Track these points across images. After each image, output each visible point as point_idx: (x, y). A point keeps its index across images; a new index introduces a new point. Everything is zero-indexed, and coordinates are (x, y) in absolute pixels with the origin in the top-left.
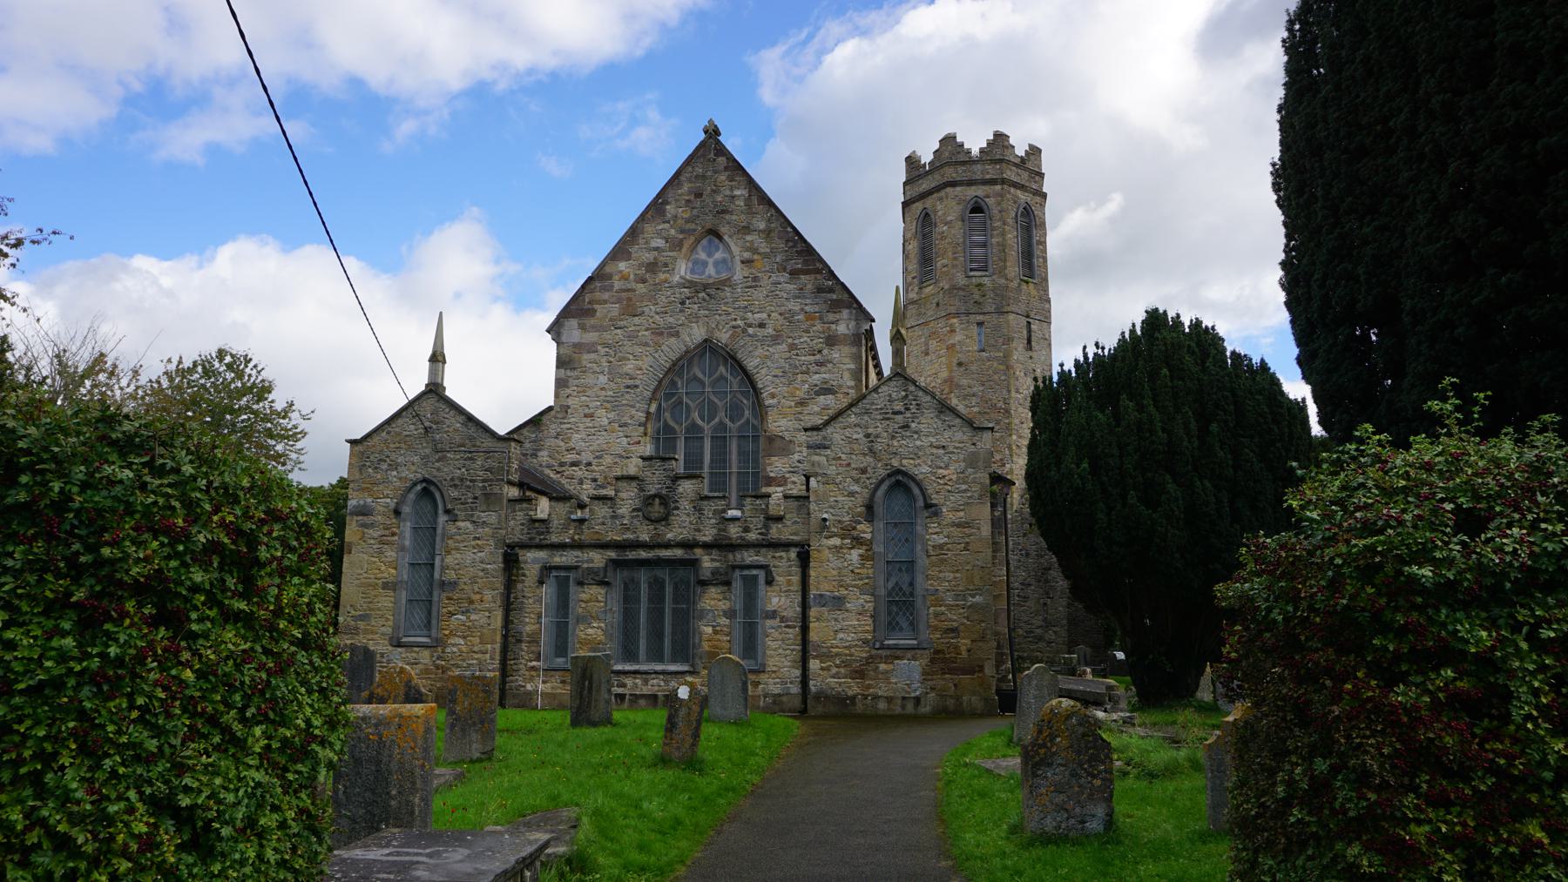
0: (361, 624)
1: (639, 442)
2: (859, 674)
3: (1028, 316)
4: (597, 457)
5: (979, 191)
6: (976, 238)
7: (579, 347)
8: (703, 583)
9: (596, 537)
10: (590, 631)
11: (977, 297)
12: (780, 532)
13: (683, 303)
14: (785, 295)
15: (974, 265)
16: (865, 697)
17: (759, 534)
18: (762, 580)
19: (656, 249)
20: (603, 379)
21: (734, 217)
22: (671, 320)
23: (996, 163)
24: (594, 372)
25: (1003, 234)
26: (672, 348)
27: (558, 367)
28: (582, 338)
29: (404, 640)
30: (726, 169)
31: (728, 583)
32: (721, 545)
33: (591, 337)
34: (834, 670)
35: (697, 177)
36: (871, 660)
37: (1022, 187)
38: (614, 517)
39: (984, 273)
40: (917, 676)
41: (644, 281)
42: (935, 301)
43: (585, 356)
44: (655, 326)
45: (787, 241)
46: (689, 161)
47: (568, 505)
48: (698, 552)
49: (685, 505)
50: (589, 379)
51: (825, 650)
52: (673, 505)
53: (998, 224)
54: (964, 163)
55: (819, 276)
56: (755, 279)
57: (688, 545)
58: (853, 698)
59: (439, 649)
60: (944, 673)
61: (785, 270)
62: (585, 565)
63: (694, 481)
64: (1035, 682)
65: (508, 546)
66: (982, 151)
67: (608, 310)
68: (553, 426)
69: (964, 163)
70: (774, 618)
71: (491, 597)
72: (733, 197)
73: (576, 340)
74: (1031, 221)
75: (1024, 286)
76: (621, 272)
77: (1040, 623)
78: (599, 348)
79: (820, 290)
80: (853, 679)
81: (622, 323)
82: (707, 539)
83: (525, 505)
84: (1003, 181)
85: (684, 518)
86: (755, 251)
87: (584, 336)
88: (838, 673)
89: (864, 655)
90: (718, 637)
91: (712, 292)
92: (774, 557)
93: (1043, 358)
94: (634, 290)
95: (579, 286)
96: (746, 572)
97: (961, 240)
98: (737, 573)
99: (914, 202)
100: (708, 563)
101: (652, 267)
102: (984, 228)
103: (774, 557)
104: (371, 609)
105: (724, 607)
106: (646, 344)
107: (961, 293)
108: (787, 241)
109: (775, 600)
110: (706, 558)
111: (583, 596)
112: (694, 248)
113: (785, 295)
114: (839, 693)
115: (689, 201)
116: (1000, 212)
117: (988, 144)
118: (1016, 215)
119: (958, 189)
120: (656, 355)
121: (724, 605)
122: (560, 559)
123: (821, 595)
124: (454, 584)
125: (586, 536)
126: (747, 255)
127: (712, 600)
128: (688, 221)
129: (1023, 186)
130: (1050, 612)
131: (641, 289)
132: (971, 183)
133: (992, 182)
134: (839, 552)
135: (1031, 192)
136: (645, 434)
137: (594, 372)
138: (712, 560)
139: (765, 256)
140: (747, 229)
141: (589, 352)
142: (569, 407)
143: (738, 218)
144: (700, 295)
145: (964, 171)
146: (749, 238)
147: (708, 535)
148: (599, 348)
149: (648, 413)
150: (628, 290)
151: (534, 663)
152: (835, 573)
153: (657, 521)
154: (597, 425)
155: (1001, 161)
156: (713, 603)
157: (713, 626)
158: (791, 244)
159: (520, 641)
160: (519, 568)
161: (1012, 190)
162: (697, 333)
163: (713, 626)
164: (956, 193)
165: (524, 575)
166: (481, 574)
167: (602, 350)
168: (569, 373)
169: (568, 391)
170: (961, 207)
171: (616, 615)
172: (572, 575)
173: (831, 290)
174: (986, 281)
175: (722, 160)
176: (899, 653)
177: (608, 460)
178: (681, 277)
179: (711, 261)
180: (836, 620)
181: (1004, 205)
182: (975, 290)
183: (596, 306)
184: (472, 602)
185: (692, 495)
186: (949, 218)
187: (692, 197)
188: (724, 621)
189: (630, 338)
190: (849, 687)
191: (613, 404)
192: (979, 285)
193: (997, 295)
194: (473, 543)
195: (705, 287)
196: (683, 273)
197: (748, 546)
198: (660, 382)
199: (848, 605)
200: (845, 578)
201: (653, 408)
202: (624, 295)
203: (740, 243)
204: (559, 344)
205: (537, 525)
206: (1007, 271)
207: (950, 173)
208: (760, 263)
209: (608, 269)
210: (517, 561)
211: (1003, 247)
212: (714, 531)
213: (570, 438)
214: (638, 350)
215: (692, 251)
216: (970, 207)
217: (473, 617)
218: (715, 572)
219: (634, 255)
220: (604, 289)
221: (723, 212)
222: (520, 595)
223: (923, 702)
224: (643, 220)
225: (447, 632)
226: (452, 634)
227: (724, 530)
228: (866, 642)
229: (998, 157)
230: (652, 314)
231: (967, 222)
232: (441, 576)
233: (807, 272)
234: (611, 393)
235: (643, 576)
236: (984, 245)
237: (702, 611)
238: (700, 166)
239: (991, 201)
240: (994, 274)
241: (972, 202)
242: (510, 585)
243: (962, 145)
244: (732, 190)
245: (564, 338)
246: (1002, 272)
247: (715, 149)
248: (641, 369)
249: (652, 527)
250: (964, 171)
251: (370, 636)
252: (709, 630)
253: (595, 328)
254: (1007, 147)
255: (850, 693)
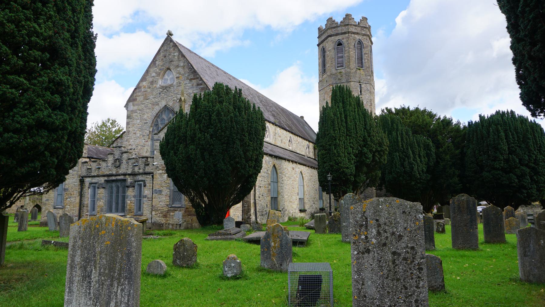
0: (47, 202)
1: (147, 141)
2: (165, 216)
3: (360, 82)
4: (136, 147)
5: (340, 37)
6: (339, 55)
7: (132, 111)
8: (128, 187)
9: (102, 173)
10: (100, 203)
11: (339, 77)
12: (148, 169)
13: (160, 94)
14: (188, 88)
15: (339, 65)
16: (166, 224)
17: (143, 170)
18: (143, 185)
19: (153, 77)
20: (138, 121)
21: (174, 63)
22: (157, 100)
23: (346, 26)
24: (136, 119)
25: (349, 52)
26: (157, 109)
27: (127, 118)
28: (133, 108)
29: (56, 207)
30: (173, 46)
31: (134, 187)
32: (133, 174)
33: (136, 108)
34: (159, 215)
35: (165, 50)
36: (168, 211)
37: (357, 34)
38: (107, 166)
39: (342, 68)
40: (181, 217)
41: (150, 88)
42: (326, 80)
43: (134, 114)
44: (152, 102)
45: (189, 69)
46: (163, 45)
47: (96, 163)
48: (127, 176)
49: (124, 161)
50: (135, 122)
51: (156, 208)
52: (121, 162)
53: (347, 49)
54: (334, 27)
55: (198, 80)
56: (180, 83)
57: (125, 175)
58: (163, 224)
59: (64, 209)
60: (188, 216)
61: (188, 79)
62: (100, 182)
63: (127, 154)
64: (63, 219)
65: (81, 177)
66: (341, 22)
67: (140, 99)
68: (125, 138)
69: (334, 27)
70: (146, 198)
71: (76, 193)
72: (174, 56)
73: (132, 109)
74: (362, 46)
75: (358, 71)
76: (143, 85)
77: (363, 197)
78: (138, 111)
79: (198, 85)
80: (163, 218)
81: (143, 102)
82: (130, 172)
83: (86, 164)
84: (349, 32)
85: (124, 166)
86: (180, 73)
87: (134, 108)
88: (159, 216)
89: (167, 210)
90: (131, 204)
91: (168, 89)
92: (146, 178)
93: (367, 97)
94: (147, 91)
95: (132, 92)
96: (139, 183)
97: (334, 56)
98: (137, 183)
99: (320, 44)
100: (129, 180)
101: (152, 83)
102: (342, 51)
103: (146, 178)
104: (49, 198)
105: (133, 194)
106: (150, 109)
107: (334, 76)
108: (189, 69)
109: (146, 192)
110: (129, 179)
111: (99, 192)
112: (164, 75)
113: (188, 88)
114: (159, 223)
115: (162, 59)
116: (348, 44)
117: (343, 19)
118: (355, 45)
119: (333, 37)
120: (152, 112)
121: (133, 194)
122: (95, 180)
123: (156, 190)
124: (67, 189)
125: (100, 173)
126: (178, 75)
127: (131, 193)
128: (162, 66)
129: (357, 33)
130: (366, 192)
131: (149, 90)
132: (337, 35)
133: (345, 33)
134: (161, 175)
135: (361, 35)
136: (149, 138)
137: (136, 119)
138: (131, 179)
139: (183, 75)
140: (178, 66)
141: (135, 113)
142: (129, 131)
143: (175, 63)
144: (165, 90)
145: (335, 31)
146: (178, 69)
147: (129, 172)
148: (138, 111)
149: (150, 131)
150: (145, 91)
151: (87, 213)
152: (160, 182)
153: (117, 167)
154: (137, 136)
155: (348, 25)
156: (130, 193)
157: (130, 201)
158: (190, 70)
159: (84, 206)
160: (84, 184)
161: (353, 35)
162: (163, 104)
163: (130, 201)
164: (332, 39)
165: (85, 186)
166: (74, 186)
167: (138, 112)
168: (130, 120)
169: (129, 126)
170: (334, 44)
171: (107, 198)
172: (97, 185)
173: (201, 84)
174: (343, 70)
175: (172, 44)
176: (176, 209)
177: (139, 147)
178: (160, 85)
179: (169, 78)
180: (159, 198)
181: (350, 42)
182: (339, 75)
183: (137, 98)
184: (71, 195)
185: (126, 159)
186: (330, 49)
187: (163, 58)
188: (133, 199)
189: (146, 107)
190: (162, 221)
191: (141, 129)
192: (341, 72)
193: (346, 75)
194: (72, 176)
195: (166, 87)
196: (160, 84)
197: (139, 174)
198: (153, 121)
199: (163, 193)
200: (162, 184)
201: (151, 130)
202: (144, 93)
203: (176, 71)
204: (127, 111)
205: (89, 170)
206: (350, 66)
207: (330, 32)
208: (182, 78)
209: (140, 85)
210: (84, 181)
211: (349, 57)
212: (131, 170)
213: (130, 141)
214: (148, 110)
215: (163, 76)
216: (337, 44)
217: (72, 199)
218: (131, 183)
219: (147, 80)
220: (139, 92)
221: (171, 61)
222: (84, 192)
223: (182, 226)
224: (150, 67)
225: (65, 204)
226: (67, 205)
227: (134, 169)
228: (167, 205)
229: (347, 23)
230: (151, 99)
231: (336, 49)
232: (64, 187)
233: (194, 79)
234: (140, 126)
235: (114, 185)
236: (342, 57)
237: (127, 196)
238: (166, 46)
239: (344, 41)
240: (346, 68)
241: (337, 42)
242: (82, 189)
243: (334, 21)
244: (174, 54)
245: (129, 109)
246: (348, 67)
247: (170, 40)
248: (148, 117)
249: (116, 169)
250: (335, 31)
251: (49, 206)
252: (129, 202)
253: (138, 105)
254: (351, 19)
255: (162, 223)
